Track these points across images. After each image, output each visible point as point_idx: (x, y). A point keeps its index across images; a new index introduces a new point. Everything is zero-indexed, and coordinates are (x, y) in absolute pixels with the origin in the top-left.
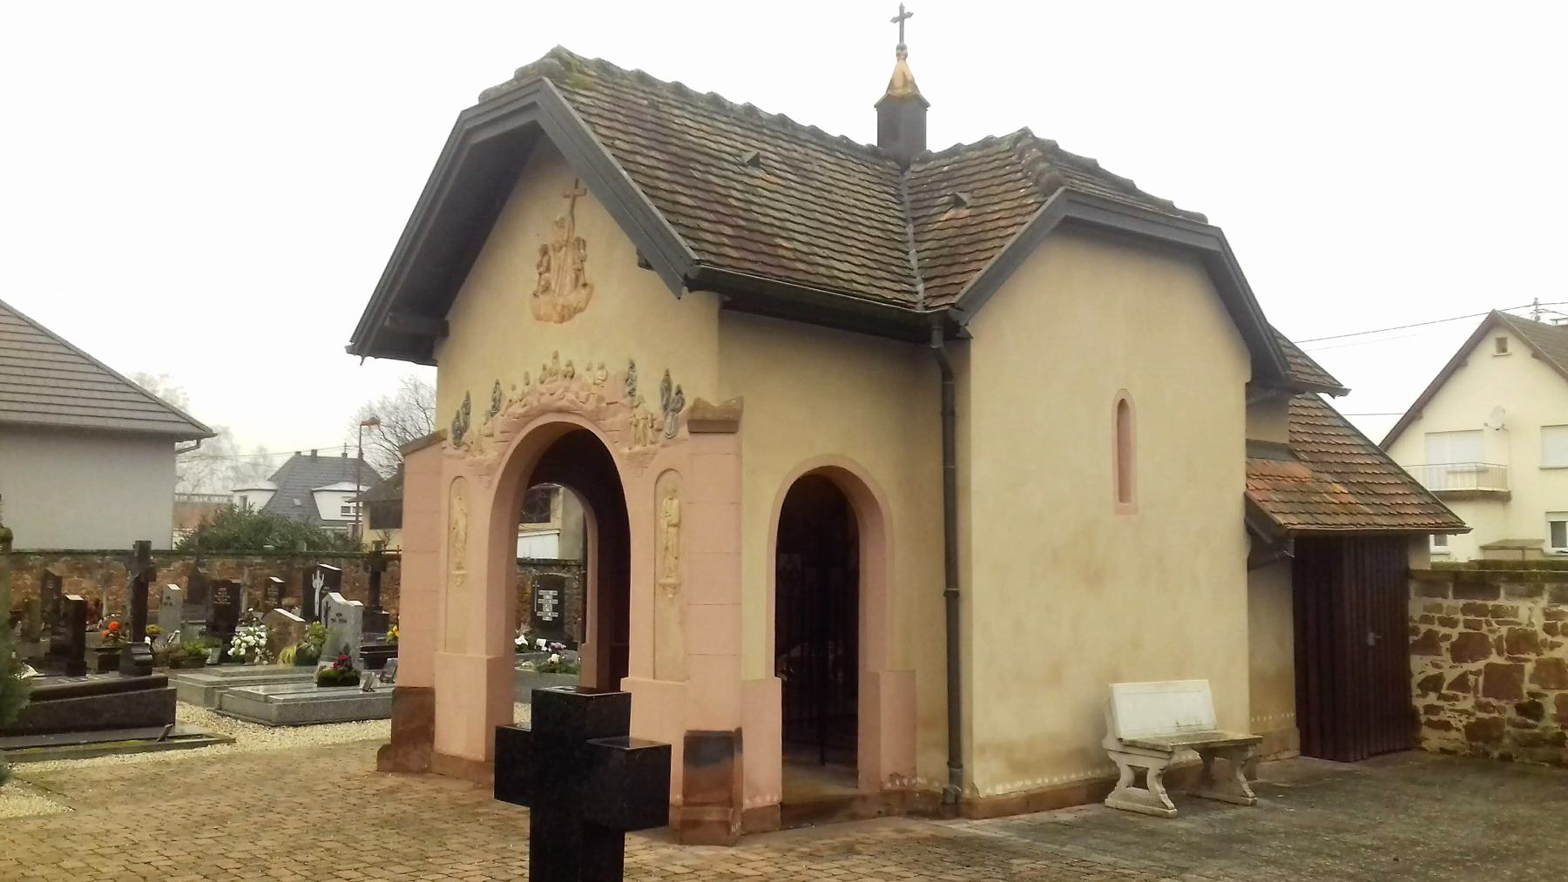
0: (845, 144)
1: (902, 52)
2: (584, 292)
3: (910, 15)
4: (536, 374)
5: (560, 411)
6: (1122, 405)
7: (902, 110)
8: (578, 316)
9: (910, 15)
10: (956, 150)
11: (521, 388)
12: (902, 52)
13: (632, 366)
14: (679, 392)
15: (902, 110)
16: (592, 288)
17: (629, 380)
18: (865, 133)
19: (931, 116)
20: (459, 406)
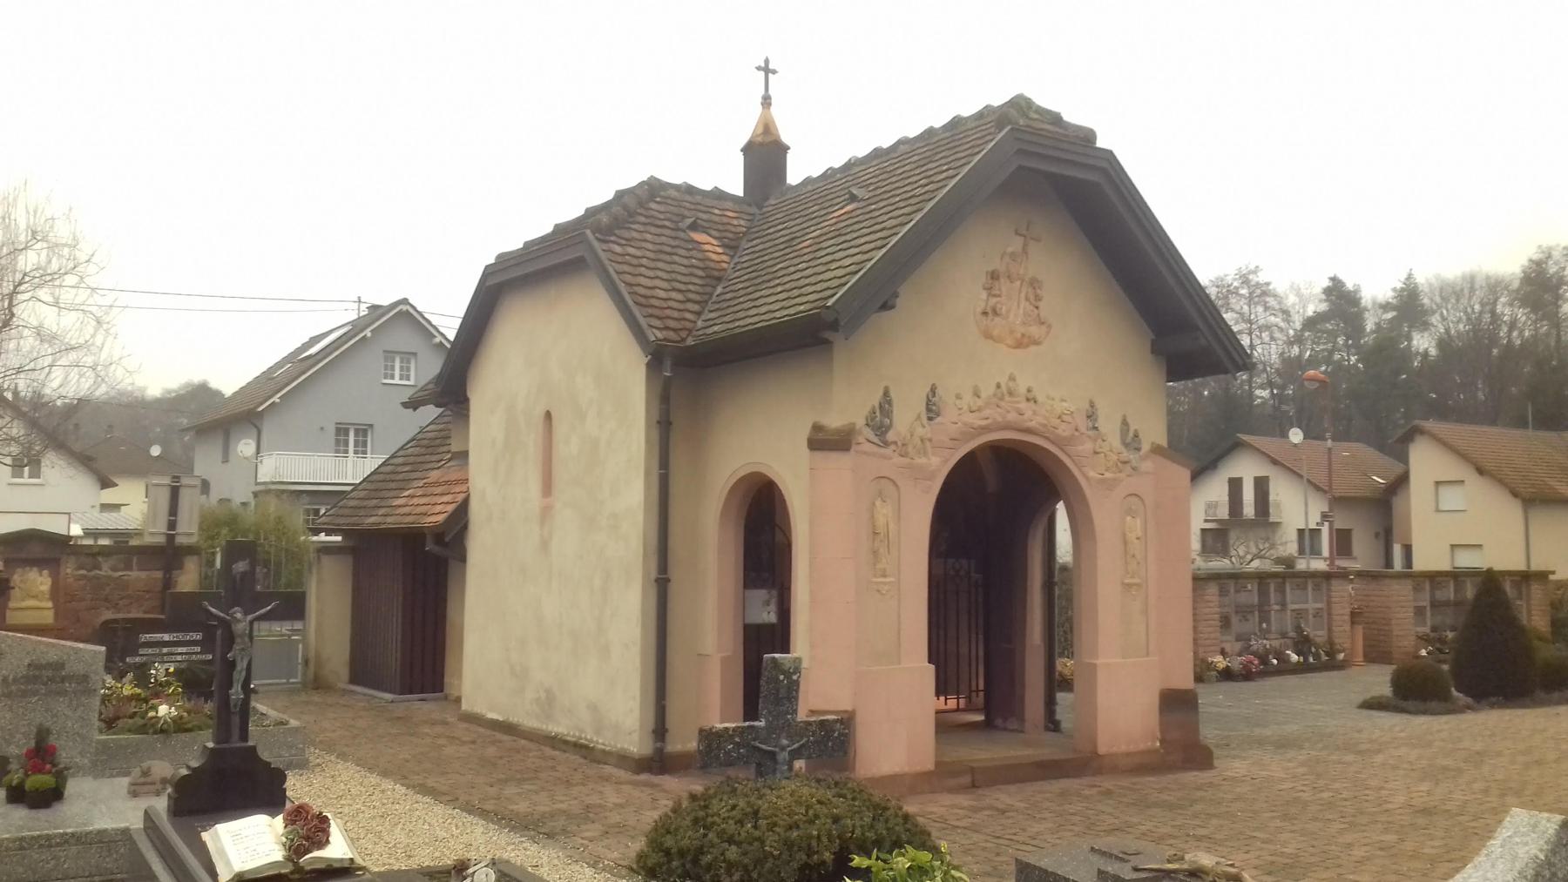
0: (718, 195)
1: (766, 101)
2: (1044, 328)
3: (767, 61)
4: (988, 391)
5: (1029, 431)
6: (548, 415)
7: (765, 155)
8: (1033, 348)
9: (767, 61)
10: (808, 181)
11: (968, 398)
12: (766, 101)
13: (1092, 405)
14: (1136, 436)
15: (765, 155)
16: (1049, 326)
17: (1091, 416)
18: (735, 185)
19: (790, 156)
20: (876, 399)
